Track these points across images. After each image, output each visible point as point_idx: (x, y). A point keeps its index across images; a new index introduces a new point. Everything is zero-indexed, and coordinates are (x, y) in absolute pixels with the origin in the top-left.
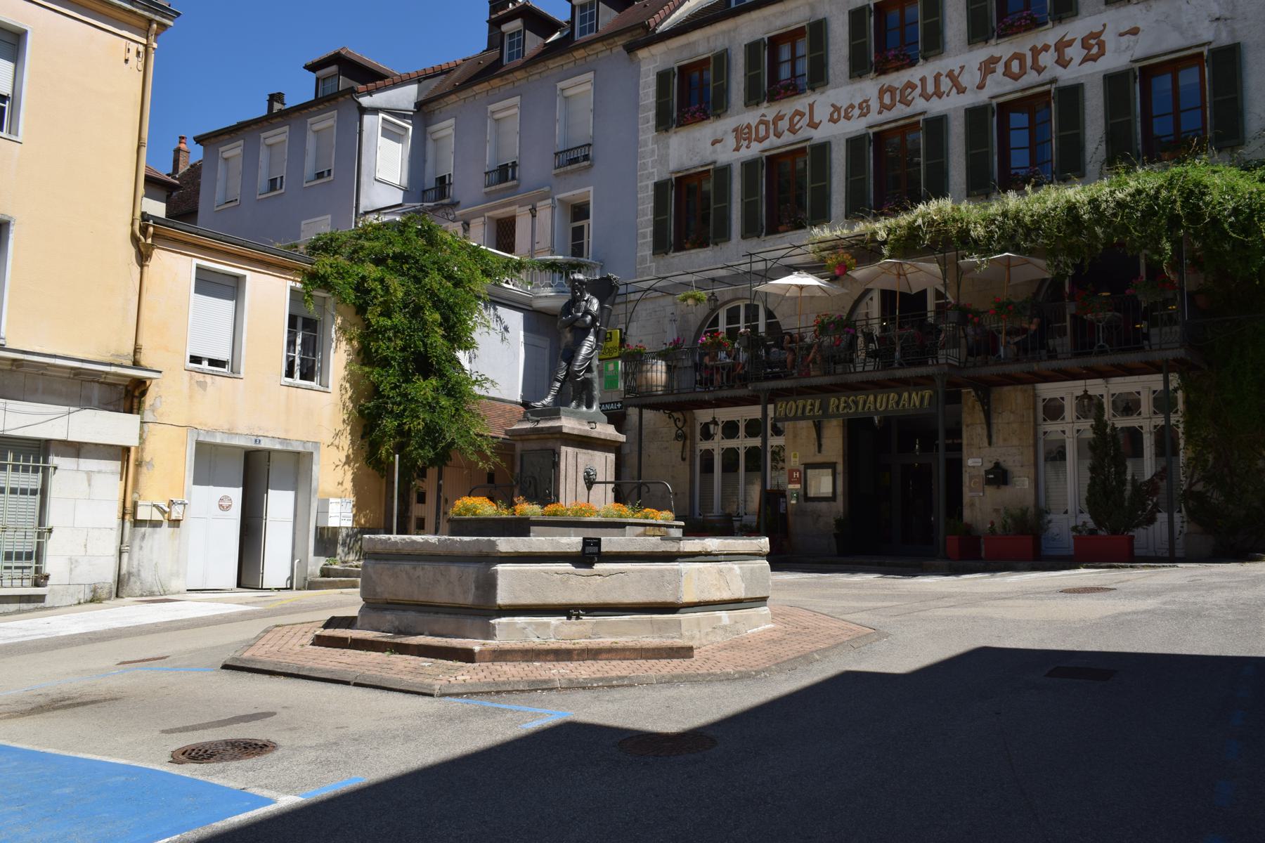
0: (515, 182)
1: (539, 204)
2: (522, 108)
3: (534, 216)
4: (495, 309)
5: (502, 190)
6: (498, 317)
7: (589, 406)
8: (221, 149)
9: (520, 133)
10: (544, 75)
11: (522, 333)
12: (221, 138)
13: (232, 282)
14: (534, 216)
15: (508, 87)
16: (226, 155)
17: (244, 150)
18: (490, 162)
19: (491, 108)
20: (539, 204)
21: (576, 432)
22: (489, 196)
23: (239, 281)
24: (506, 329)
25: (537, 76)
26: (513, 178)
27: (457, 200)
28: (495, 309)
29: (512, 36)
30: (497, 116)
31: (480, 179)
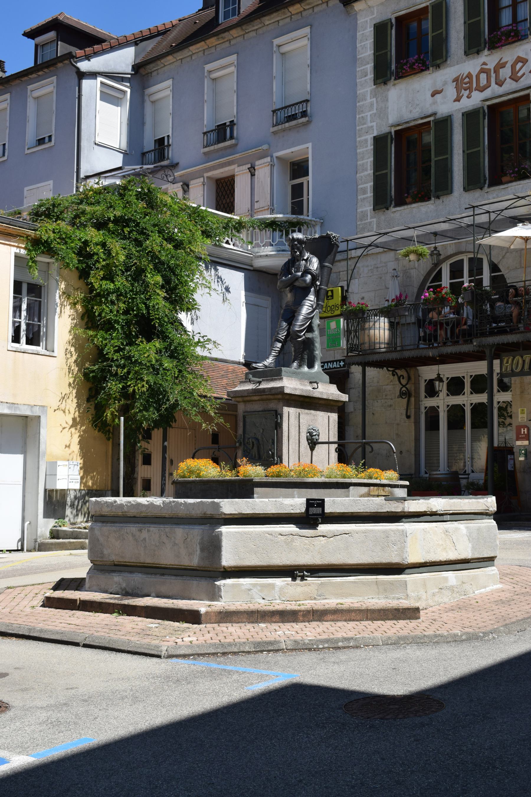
0: (233, 141)
1: (257, 163)
2: (239, 67)
3: (253, 175)
6: (219, 277)
9: (238, 92)
10: (260, 31)
11: (243, 293)
14: (253, 175)
18: (208, 122)
19: (208, 67)
20: (257, 163)
21: (298, 393)
24: (227, 289)
25: (253, 34)
26: (232, 137)
27: (175, 161)
28: (216, 270)
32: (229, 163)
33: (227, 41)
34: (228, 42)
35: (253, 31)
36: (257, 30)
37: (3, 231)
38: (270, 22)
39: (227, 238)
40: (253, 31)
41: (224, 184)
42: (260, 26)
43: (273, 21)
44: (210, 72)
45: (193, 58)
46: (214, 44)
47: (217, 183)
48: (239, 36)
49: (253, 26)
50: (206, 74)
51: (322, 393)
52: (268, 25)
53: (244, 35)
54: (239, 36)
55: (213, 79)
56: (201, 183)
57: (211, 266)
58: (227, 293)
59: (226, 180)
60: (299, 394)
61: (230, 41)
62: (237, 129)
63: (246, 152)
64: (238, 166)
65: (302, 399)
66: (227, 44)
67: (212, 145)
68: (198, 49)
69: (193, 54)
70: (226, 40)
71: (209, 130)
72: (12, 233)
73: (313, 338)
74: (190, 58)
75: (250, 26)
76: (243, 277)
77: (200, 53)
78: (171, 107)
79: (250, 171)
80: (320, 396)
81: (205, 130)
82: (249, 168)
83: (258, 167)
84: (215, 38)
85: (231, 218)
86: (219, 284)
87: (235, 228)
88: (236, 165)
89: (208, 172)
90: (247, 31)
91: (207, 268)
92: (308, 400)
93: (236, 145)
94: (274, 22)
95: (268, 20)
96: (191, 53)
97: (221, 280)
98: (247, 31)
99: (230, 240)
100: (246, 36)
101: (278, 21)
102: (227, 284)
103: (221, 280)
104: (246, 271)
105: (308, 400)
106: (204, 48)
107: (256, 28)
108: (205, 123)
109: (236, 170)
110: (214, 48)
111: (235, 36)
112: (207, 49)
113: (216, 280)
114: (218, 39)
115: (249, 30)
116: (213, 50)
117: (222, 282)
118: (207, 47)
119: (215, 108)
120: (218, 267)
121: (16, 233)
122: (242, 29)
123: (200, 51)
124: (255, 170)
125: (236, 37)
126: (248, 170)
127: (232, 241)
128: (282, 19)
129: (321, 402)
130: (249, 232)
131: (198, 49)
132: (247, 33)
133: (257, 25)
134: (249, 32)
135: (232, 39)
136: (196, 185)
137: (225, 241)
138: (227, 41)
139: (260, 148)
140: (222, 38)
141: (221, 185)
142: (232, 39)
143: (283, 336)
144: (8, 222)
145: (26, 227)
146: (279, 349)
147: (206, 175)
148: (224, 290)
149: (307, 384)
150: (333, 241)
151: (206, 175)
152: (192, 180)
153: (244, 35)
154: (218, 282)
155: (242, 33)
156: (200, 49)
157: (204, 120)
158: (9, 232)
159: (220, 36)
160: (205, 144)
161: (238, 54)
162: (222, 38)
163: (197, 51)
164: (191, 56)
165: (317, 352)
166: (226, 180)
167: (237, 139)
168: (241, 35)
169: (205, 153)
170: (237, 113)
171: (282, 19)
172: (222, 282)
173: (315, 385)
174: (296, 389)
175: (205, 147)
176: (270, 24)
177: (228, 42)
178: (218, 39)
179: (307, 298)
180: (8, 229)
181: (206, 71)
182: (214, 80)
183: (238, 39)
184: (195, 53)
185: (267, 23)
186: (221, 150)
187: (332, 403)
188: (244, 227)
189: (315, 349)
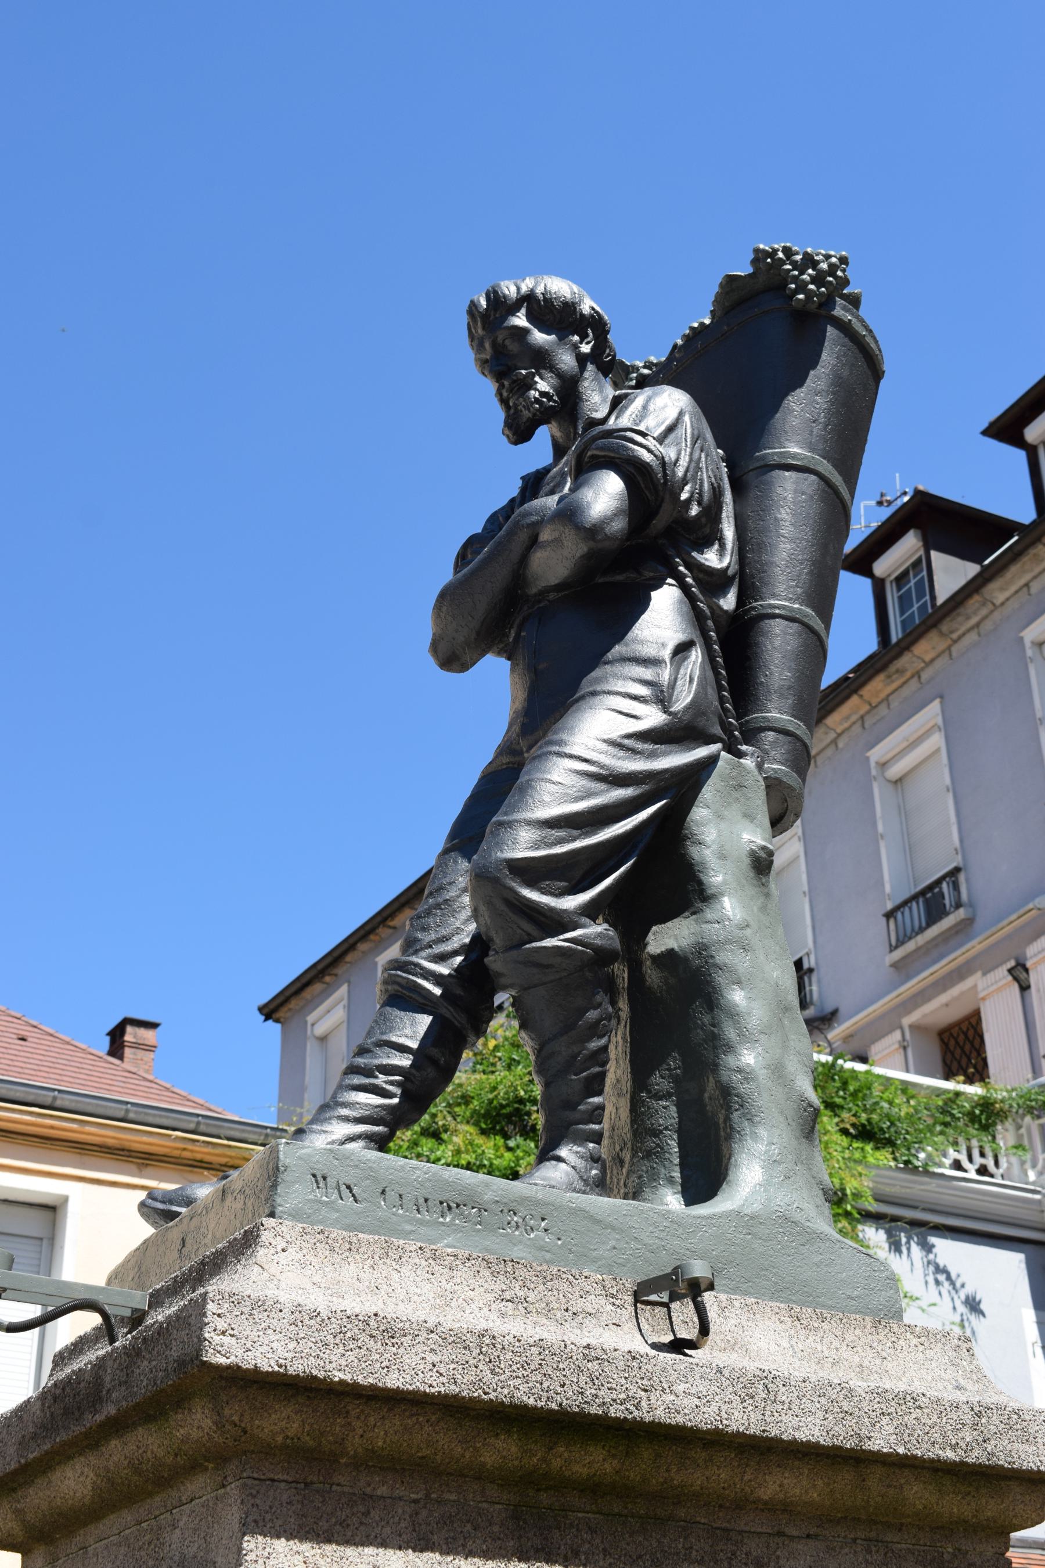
0: (961, 913)
1: (1031, 950)
2: (949, 727)
3: (1024, 988)
4: (928, 1248)
5: (934, 942)
6: (939, 1269)
7: (704, 1178)
8: (310, 1019)
9: (955, 790)
10: (988, 625)
11: (1029, 1315)
12: (307, 994)
13: (32, 1224)
14: (1024, 988)
15: (906, 691)
16: (320, 1030)
17: (349, 1008)
18: (893, 883)
19: (876, 754)
20: (1031, 950)
21: (409, 1371)
22: (903, 969)
23: (52, 1210)
24: (973, 1305)
25: (973, 636)
26: (958, 905)
27: (829, 1008)
28: (928, 1248)
29: (901, 579)
30: (896, 770)
31: (878, 930)
32: (960, 974)
33: (912, 677)
34: (916, 679)
35: (969, 630)
36: (977, 625)
37: (176, 1153)
38: (1007, 594)
39: (952, 1154)
40: (969, 630)
41: (962, 1037)
42: (984, 612)
43: (1013, 588)
44: (883, 765)
45: (841, 745)
46: (883, 695)
47: (942, 1040)
48: (938, 656)
49: (968, 618)
50: (874, 772)
51: (764, 1385)
52: (1003, 604)
53: (949, 648)
54: (938, 656)
55: (896, 782)
56: (897, 1046)
57: (909, 1239)
58: (973, 1318)
59: (964, 1027)
60: (435, 1384)
61: (917, 674)
62: (967, 880)
63: (994, 929)
64: (984, 974)
65: (501, 1450)
66: (914, 682)
67: (910, 938)
68: (847, 718)
69: (839, 735)
70: (908, 674)
71: (899, 900)
72: (207, 1158)
73: (702, 949)
74: (833, 746)
75: (960, 619)
76: (1023, 1266)
77: (854, 728)
78: (804, 877)
79: (1016, 979)
80: (741, 1419)
81: (889, 906)
82: (1010, 971)
83: (1035, 960)
84: (881, 677)
85: (957, 1094)
86: (944, 1292)
87: (972, 1118)
88: (979, 974)
89: (909, 1012)
90: (954, 636)
91: (895, 1246)
92: (592, 1461)
93: (968, 923)
94: (1017, 592)
95: (1002, 589)
96: (833, 735)
97: (949, 1278)
98: (954, 636)
99: (963, 1158)
100: (954, 649)
101: (1027, 585)
102: (969, 1290)
103: (949, 1278)
104: (1029, 1247)
105: (592, 1461)
106: (862, 712)
107: (974, 620)
108: (888, 888)
109: (980, 987)
110: (884, 706)
111: (927, 658)
112: (868, 712)
113: (931, 1279)
114: (889, 677)
115: (960, 632)
116: (883, 710)
117: (953, 1284)
118: (867, 707)
119: (910, 849)
120: (933, 1240)
121: (224, 1160)
122: (942, 634)
123: (854, 723)
124: (1027, 970)
125: (932, 661)
126: (1010, 978)
127: (970, 1159)
128: (1035, 577)
129: (774, 1484)
130: (1023, 1131)
131: (847, 718)
132: (955, 641)
133: (975, 613)
134: (960, 638)
135: (923, 669)
136: (885, 1053)
137: (947, 1162)
138: (912, 677)
139: (1031, 906)
140: (897, 671)
141: (952, 1042)
142: (923, 669)
143: (441, 958)
144: (192, 1126)
145: (252, 1137)
146: (405, 1061)
147: (906, 1021)
148: (962, 1309)
149: (595, 1302)
150: (802, 287)
151: (906, 1021)
152: (873, 1042)
153: (949, 648)
154: (937, 1282)
155: (943, 645)
156: (854, 718)
157: (883, 885)
158: (199, 1156)
159: (892, 668)
160: (894, 942)
161: (941, 697)
162: (897, 671)
163: (846, 725)
164: (834, 742)
165: (749, 1058)
166: (964, 1027)
167: (971, 905)
168: (943, 652)
169: (895, 965)
170: (961, 841)
171: (1035, 577)
172: (953, 1284)
173: (684, 1320)
174: (390, 1333)
175: (892, 949)
176: (1008, 599)
177: (916, 679)
178: (889, 677)
179: (618, 650)
180: (190, 1146)
181: (873, 764)
182: (898, 782)
183: (938, 664)
184: (843, 732)
185: (1000, 597)
186: (936, 946)
187: (917, 1494)
188: (1002, 1115)
189: (730, 1033)
